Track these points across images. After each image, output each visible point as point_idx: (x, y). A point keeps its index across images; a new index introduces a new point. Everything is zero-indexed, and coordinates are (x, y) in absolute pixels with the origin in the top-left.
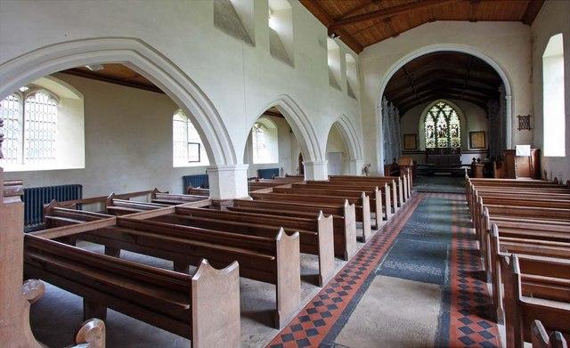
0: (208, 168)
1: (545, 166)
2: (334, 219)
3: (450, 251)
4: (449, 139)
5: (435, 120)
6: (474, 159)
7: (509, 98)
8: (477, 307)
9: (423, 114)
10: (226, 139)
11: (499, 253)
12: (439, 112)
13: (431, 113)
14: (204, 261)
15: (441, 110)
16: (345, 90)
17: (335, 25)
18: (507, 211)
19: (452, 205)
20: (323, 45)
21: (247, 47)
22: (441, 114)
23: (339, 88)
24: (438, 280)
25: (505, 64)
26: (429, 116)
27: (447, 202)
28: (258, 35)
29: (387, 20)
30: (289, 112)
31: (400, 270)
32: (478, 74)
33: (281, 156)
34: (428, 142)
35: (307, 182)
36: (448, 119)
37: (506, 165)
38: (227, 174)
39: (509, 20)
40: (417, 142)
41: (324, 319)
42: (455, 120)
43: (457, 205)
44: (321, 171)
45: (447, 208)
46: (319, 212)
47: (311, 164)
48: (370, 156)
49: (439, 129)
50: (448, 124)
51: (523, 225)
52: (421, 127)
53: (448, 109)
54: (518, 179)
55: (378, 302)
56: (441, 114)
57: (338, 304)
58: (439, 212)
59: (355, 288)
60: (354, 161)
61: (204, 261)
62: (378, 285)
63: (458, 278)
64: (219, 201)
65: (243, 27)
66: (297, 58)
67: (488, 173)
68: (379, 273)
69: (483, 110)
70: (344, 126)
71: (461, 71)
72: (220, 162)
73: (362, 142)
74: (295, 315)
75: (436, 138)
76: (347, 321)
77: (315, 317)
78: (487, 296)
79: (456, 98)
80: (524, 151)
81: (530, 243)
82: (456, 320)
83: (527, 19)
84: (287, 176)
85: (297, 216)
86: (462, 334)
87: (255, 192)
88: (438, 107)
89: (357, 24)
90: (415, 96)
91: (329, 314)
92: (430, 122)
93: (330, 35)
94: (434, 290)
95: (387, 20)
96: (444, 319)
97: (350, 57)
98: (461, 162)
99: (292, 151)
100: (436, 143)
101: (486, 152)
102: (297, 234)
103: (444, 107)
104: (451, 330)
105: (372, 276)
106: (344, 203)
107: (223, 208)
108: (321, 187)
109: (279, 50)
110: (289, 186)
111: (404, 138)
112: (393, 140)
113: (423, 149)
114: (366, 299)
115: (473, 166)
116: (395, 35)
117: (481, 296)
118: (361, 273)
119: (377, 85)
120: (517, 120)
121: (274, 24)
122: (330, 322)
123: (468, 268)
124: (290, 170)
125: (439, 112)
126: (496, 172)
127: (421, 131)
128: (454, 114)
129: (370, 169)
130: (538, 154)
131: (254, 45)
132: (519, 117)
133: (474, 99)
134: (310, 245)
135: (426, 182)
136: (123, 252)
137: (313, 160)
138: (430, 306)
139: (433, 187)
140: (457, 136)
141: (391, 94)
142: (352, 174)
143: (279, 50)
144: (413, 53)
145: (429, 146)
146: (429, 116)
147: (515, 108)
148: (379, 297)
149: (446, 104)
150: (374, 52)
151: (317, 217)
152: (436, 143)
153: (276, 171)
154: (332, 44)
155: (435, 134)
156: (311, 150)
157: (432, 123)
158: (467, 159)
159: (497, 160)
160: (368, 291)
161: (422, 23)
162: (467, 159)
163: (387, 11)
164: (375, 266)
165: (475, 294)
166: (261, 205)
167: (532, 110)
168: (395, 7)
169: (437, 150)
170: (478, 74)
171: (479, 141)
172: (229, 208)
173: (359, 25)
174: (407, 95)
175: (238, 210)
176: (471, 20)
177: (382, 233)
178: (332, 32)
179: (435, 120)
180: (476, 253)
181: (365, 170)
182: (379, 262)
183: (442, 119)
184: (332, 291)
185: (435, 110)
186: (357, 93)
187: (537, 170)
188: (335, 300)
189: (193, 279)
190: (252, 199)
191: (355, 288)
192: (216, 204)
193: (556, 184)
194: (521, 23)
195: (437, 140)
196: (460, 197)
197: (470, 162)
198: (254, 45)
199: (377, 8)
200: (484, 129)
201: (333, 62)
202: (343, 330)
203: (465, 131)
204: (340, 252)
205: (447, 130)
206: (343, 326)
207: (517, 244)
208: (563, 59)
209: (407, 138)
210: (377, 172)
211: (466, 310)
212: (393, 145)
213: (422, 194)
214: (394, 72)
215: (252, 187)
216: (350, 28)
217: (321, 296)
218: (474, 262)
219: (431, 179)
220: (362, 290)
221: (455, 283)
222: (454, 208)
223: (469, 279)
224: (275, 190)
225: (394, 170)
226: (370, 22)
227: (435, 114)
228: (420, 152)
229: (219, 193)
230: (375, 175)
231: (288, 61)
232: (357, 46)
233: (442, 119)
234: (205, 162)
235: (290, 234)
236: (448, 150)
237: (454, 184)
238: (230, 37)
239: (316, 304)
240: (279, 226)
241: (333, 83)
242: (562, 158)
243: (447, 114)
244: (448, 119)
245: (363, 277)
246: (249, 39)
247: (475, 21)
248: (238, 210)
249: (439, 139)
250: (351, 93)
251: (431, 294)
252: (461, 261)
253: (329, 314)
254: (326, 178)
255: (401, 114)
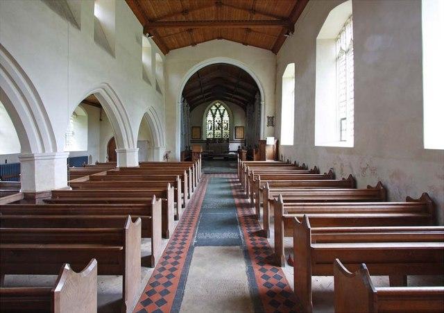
0: (20, 156)
1: (282, 152)
2: (162, 201)
3: (239, 218)
4: (222, 131)
5: (214, 116)
6: (239, 147)
7: (263, 103)
8: (266, 258)
9: (205, 112)
10: (45, 125)
11: (284, 215)
12: (216, 110)
13: (211, 110)
14: (67, 267)
15: (218, 108)
16: (154, 86)
17: (151, 26)
18: (294, 184)
19: (229, 182)
20: (139, 41)
21: (73, 29)
22: (218, 112)
23: (149, 82)
24: (237, 242)
25: (262, 79)
26: (210, 112)
27: (226, 180)
28: (84, 20)
29: (190, 30)
30: (108, 101)
31: (211, 239)
32: (244, 84)
33: (89, 147)
34: (209, 134)
35: (121, 168)
36: (222, 116)
37: (261, 151)
38: (131, 153)
39: (266, 49)
40: (201, 133)
41: (164, 298)
42: (226, 118)
43: (234, 182)
44: (132, 158)
45: (228, 185)
46: (152, 197)
47: (124, 152)
48: (169, 147)
49: (216, 123)
50: (222, 120)
51: (319, 193)
52: (204, 121)
53: (222, 108)
54: (267, 161)
55: (202, 270)
56: (218, 112)
57: (172, 280)
58: (223, 189)
59: (182, 261)
60: (158, 148)
61: (67, 267)
62: (199, 255)
63: (250, 238)
64: (35, 194)
65: (68, 7)
66: (117, 49)
67: (249, 158)
68: (196, 245)
69: (243, 111)
70: (152, 118)
71: (234, 80)
72: (36, 149)
73: (164, 129)
74: (137, 300)
75: (214, 131)
76: (183, 294)
77: (156, 298)
78: (269, 248)
79: (227, 100)
80: (271, 141)
81: (318, 205)
82: (257, 272)
83: (275, 50)
84: (97, 163)
85: (133, 202)
86: (264, 281)
87: (78, 180)
88: (216, 106)
89: (168, 29)
90: (202, 96)
91: (167, 292)
92: (210, 117)
93: (145, 33)
94: (237, 251)
95: (190, 30)
96: (250, 272)
97: (159, 57)
98: (229, 149)
99: (100, 140)
100: (214, 134)
101: (244, 141)
102: (140, 220)
103: (220, 106)
104: (257, 279)
105: (191, 249)
106: (167, 187)
107: (39, 202)
108: (132, 173)
109: (101, 37)
110: (104, 174)
111: (193, 130)
112: (185, 131)
113: (205, 139)
114: (193, 270)
115: (239, 151)
116: (194, 44)
117: (266, 249)
118: (182, 248)
119: (178, 84)
120: (266, 119)
121: (98, 12)
122: (170, 298)
123: (253, 230)
124: (98, 157)
125: (216, 110)
126: (255, 157)
127: (203, 124)
128: (226, 112)
129: (170, 155)
130: (278, 143)
131: (79, 28)
132: (268, 117)
133: (239, 102)
134: (147, 232)
135: (210, 166)
136: (8, 278)
137: (126, 147)
138: (238, 264)
139: (214, 169)
140: (227, 129)
141: (187, 94)
142: (156, 161)
143: (101, 37)
144: (208, 60)
145: (209, 137)
146: (210, 112)
147: (266, 111)
148: (202, 264)
149: (221, 104)
150: (178, 55)
151: (151, 201)
152: (214, 134)
153: (85, 159)
154: (146, 42)
155: (213, 128)
156: (125, 138)
157: (212, 119)
158: (234, 147)
159: (254, 149)
160: (192, 262)
161: (213, 39)
162: (234, 147)
163: (195, 22)
164: (192, 239)
165: (262, 248)
166: (84, 194)
167: (275, 113)
168: (198, 21)
169: (214, 140)
170: (244, 84)
171: (240, 134)
172: (45, 201)
173: (169, 30)
174: (197, 95)
175: (57, 202)
176: (244, 44)
177: (191, 209)
178: (146, 31)
179: (214, 116)
180: (256, 217)
181: (166, 156)
182: (193, 236)
183: (218, 115)
184: (163, 269)
185: (214, 108)
186: (163, 89)
187: (276, 156)
188: (168, 277)
189: (56, 290)
190: (71, 189)
191: (182, 261)
192: (30, 197)
193: (288, 164)
194: (271, 52)
195: (214, 132)
196: (233, 176)
197: (236, 149)
198: (79, 28)
199: (184, 19)
200: (244, 125)
201: (146, 59)
202: (182, 303)
203: (233, 128)
204: (165, 235)
205: (221, 125)
206: (182, 299)
207: (293, 207)
208: (294, 80)
209: (194, 130)
210: (175, 158)
211: (261, 262)
212: (185, 135)
213: (208, 175)
214: (191, 75)
215: (71, 175)
216: (161, 31)
217: (154, 276)
218: (256, 224)
219: (211, 163)
220: (188, 262)
221: (248, 242)
222: (232, 185)
223: (257, 238)
224: (92, 179)
225: (188, 156)
226: (177, 30)
227: (214, 112)
228: (202, 141)
229: (34, 186)
230: (174, 161)
231: (110, 50)
232: (165, 48)
233: (218, 115)
234: (17, 150)
235: (134, 220)
236: (221, 140)
237: (229, 167)
238: (57, 15)
239: (153, 285)
240: (128, 214)
241: (146, 78)
242: (291, 146)
243: (222, 112)
244: (222, 116)
245: (185, 250)
246: (74, 21)
247: (246, 44)
248: (57, 202)
249: (216, 131)
250: (158, 89)
251: (236, 254)
252: (248, 224)
253: (167, 292)
254: (137, 165)
255: (191, 110)
